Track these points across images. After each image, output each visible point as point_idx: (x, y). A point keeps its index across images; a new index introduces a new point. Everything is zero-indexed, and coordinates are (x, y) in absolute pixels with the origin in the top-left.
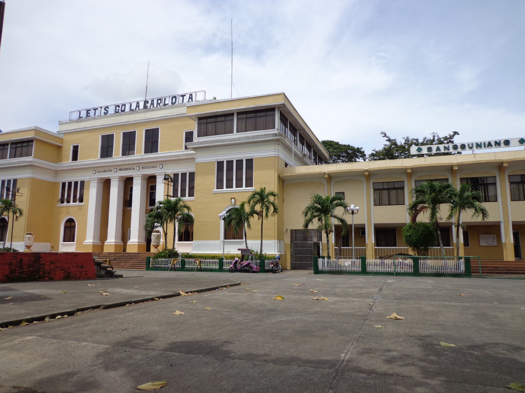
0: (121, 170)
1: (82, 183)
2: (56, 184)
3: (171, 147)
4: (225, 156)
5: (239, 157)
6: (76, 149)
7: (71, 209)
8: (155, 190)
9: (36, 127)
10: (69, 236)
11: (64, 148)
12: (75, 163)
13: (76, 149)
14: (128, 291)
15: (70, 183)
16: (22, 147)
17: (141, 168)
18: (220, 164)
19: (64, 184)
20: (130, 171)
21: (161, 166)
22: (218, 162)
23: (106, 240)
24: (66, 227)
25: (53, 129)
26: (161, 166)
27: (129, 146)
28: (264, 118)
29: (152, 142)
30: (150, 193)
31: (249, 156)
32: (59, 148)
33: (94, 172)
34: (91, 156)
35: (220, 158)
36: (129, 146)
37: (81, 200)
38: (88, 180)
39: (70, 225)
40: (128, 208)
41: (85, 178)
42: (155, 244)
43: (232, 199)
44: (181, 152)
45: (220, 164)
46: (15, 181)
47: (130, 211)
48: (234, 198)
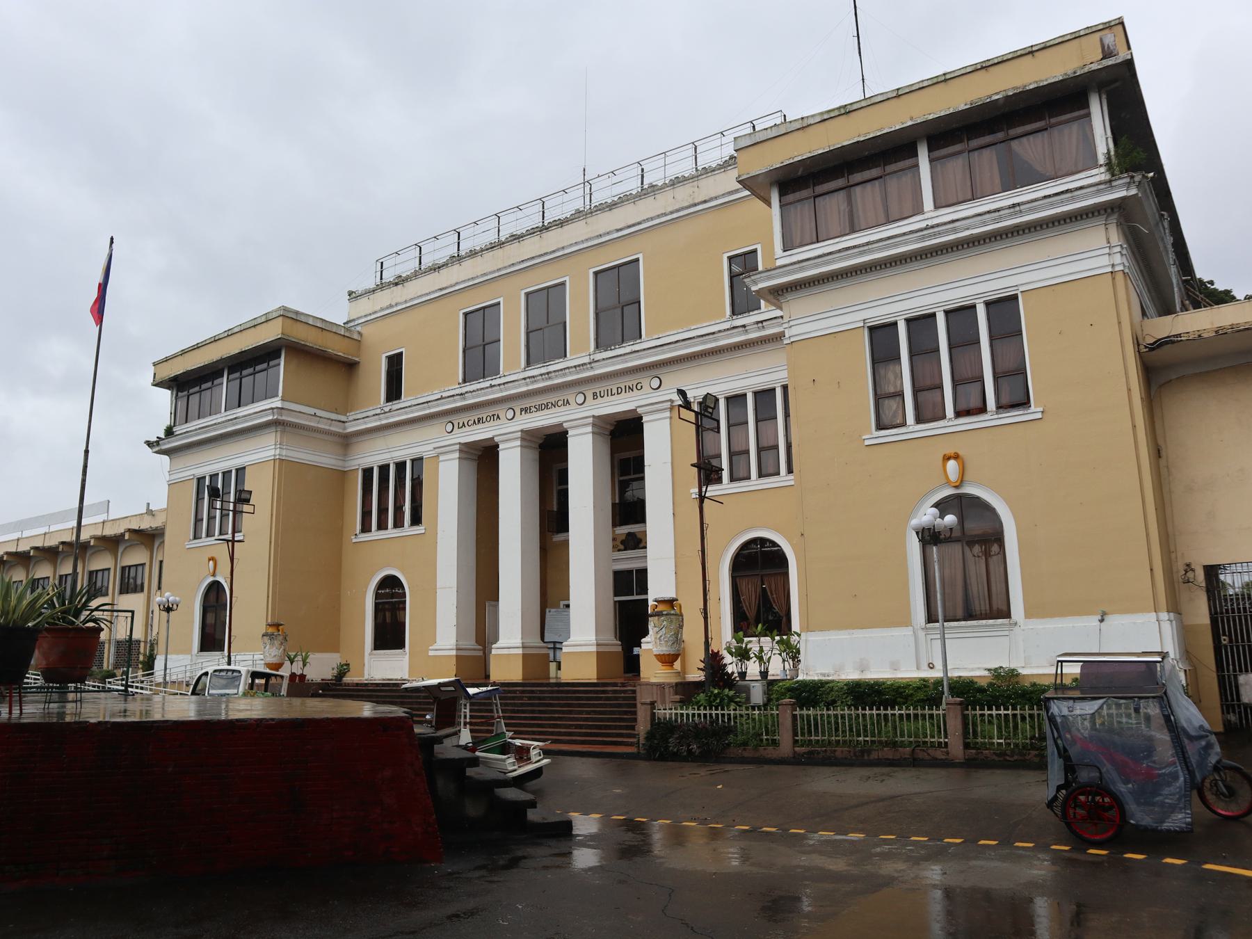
0: (526, 410)
1: (417, 461)
2: (342, 476)
3: (689, 304)
4: (897, 300)
5: (956, 296)
6: (395, 363)
7: (380, 552)
8: (643, 471)
9: (289, 316)
10: (390, 634)
11: (362, 369)
12: (396, 405)
13: (395, 363)
14: (1176, 289)
15: (384, 469)
16: (254, 374)
17: (590, 396)
18: (881, 335)
19: (368, 473)
20: (553, 410)
21: (655, 383)
22: (871, 329)
23: (496, 640)
24: (378, 608)
25: (337, 313)
26: (655, 383)
27: (546, 337)
28: (1045, 133)
29: (619, 308)
30: (620, 482)
31: (997, 286)
32: (349, 367)
33: (449, 427)
34: (436, 378)
35: (880, 313)
36: (546, 337)
37: (416, 519)
38: (433, 453)
39: (390, 598)
40: (559, 537)
41: (425, 450)
42: (664, 649)
43: (947, 458)
44: (719, 323)
45: (881, 335)
46: (241, 471)
47: (566, 543)
48: (956, 457)
